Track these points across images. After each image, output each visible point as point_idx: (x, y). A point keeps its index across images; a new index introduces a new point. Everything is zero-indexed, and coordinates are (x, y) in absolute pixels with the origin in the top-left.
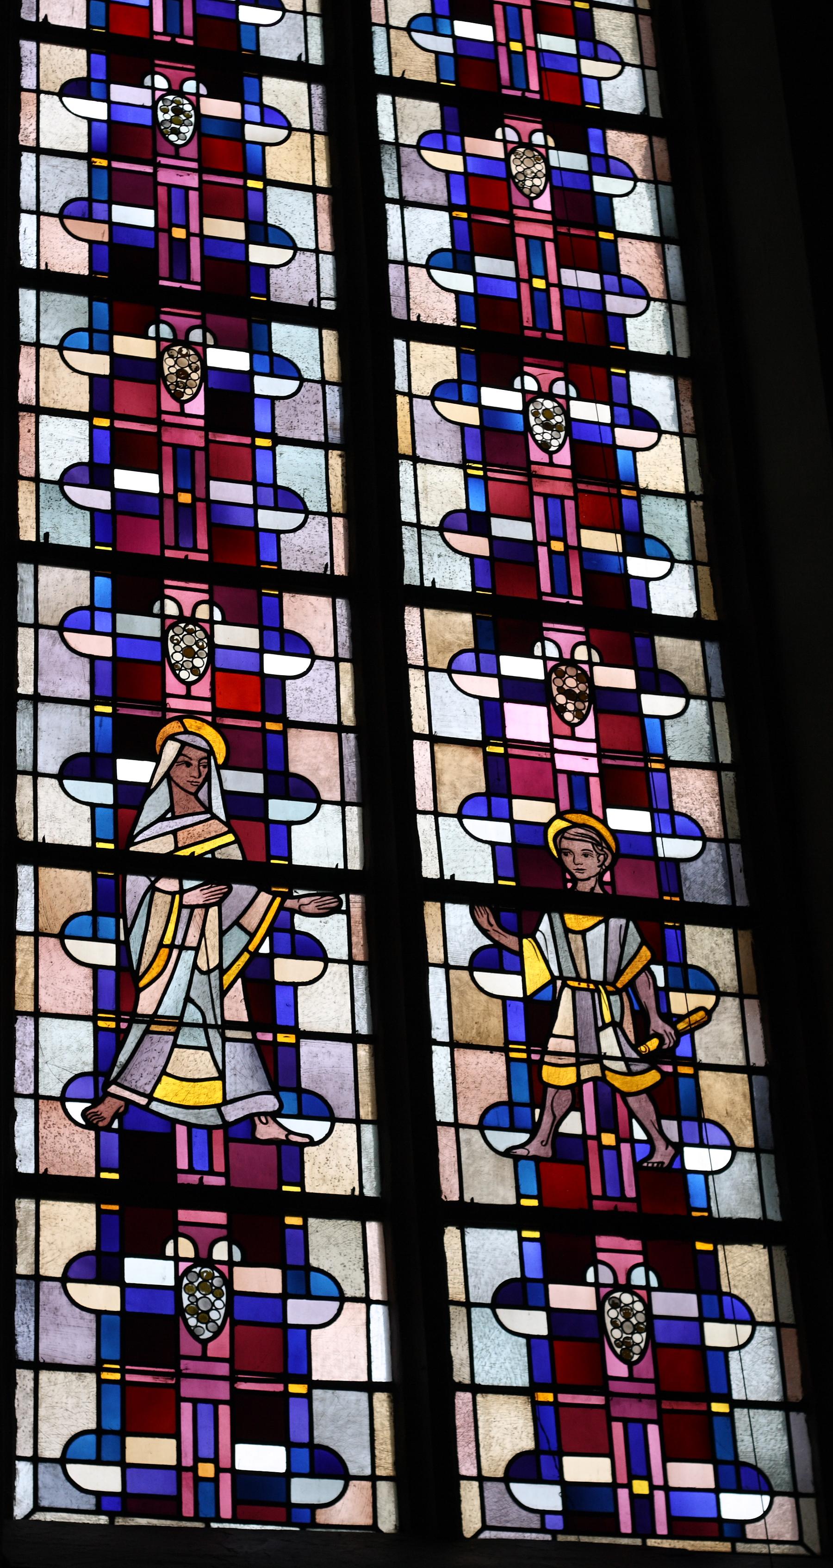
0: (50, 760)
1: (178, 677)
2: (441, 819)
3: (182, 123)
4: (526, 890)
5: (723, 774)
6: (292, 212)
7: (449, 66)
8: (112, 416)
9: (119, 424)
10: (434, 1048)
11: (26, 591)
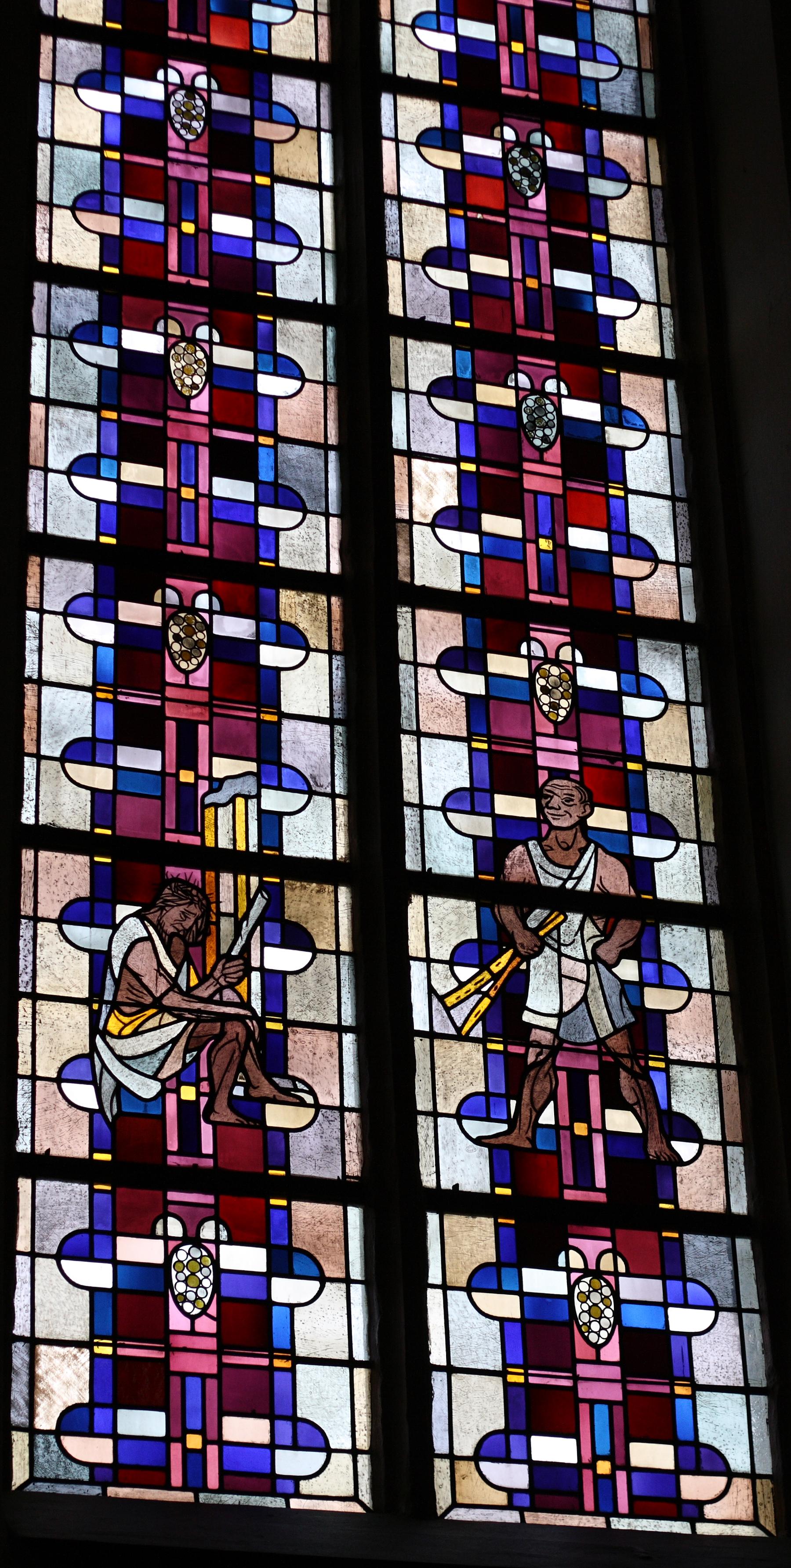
0: (59, 459)
1: (181, 1309)
2: (449, 1293)
3: (193, 118)
4: (492, 616)
5: (752, 1397)
6: (297, 208)
10: (412, 962)
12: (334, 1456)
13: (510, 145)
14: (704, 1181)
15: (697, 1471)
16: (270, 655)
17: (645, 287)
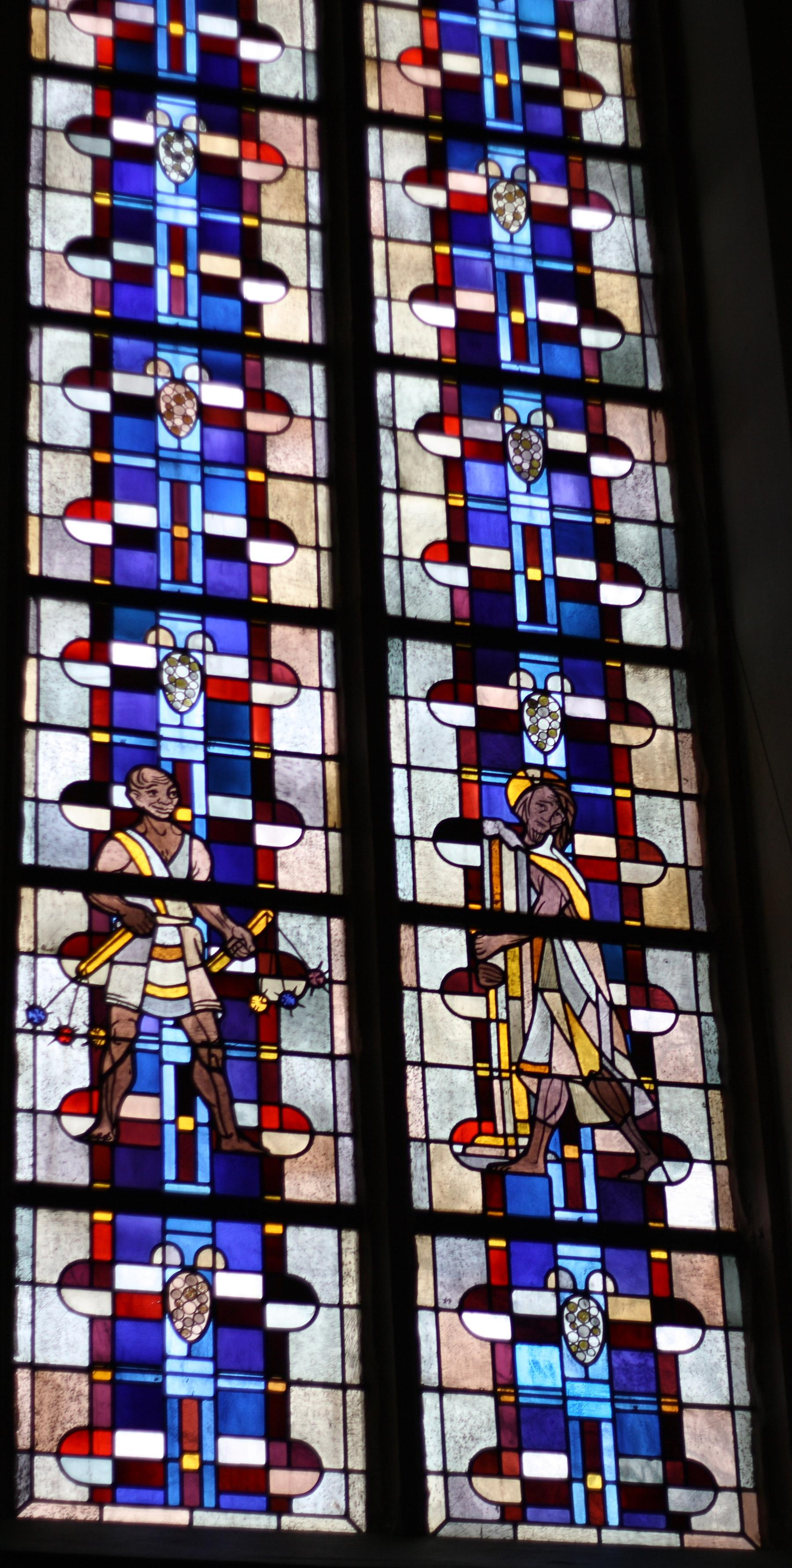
4: (483, 638)
7: (463, 601)
8: (110, 729)
9: (117, 739)
11: (26, 910)
12: (303, 690)
13: (567, 1295)
14: (692, 1200)
15: (636, 859)
16: (266, 835)
17: (663, 713)
